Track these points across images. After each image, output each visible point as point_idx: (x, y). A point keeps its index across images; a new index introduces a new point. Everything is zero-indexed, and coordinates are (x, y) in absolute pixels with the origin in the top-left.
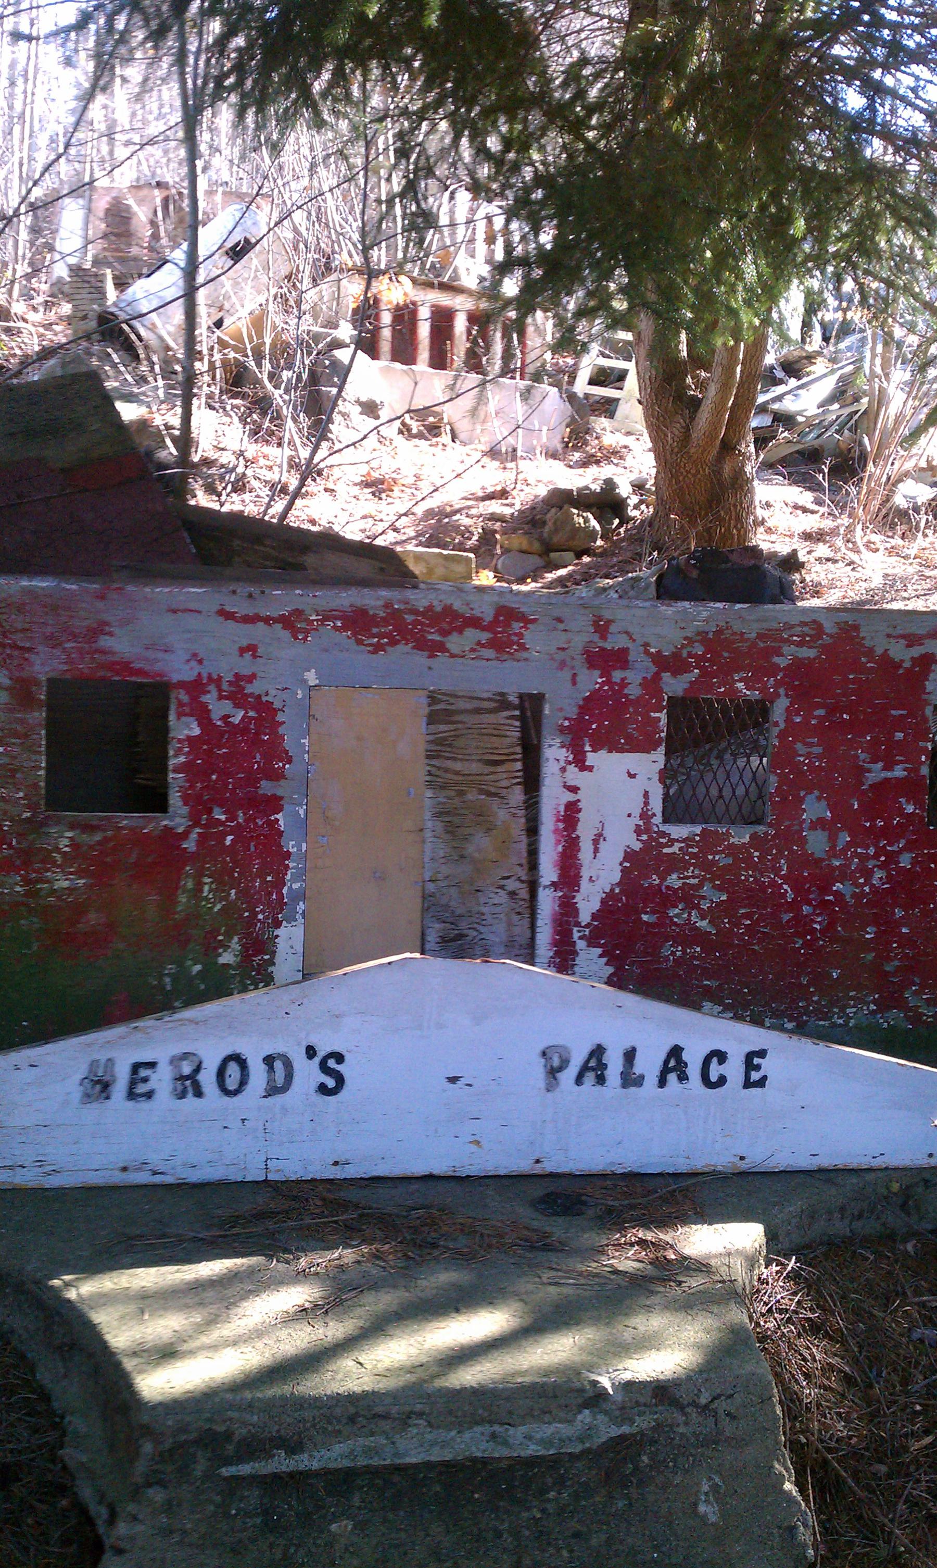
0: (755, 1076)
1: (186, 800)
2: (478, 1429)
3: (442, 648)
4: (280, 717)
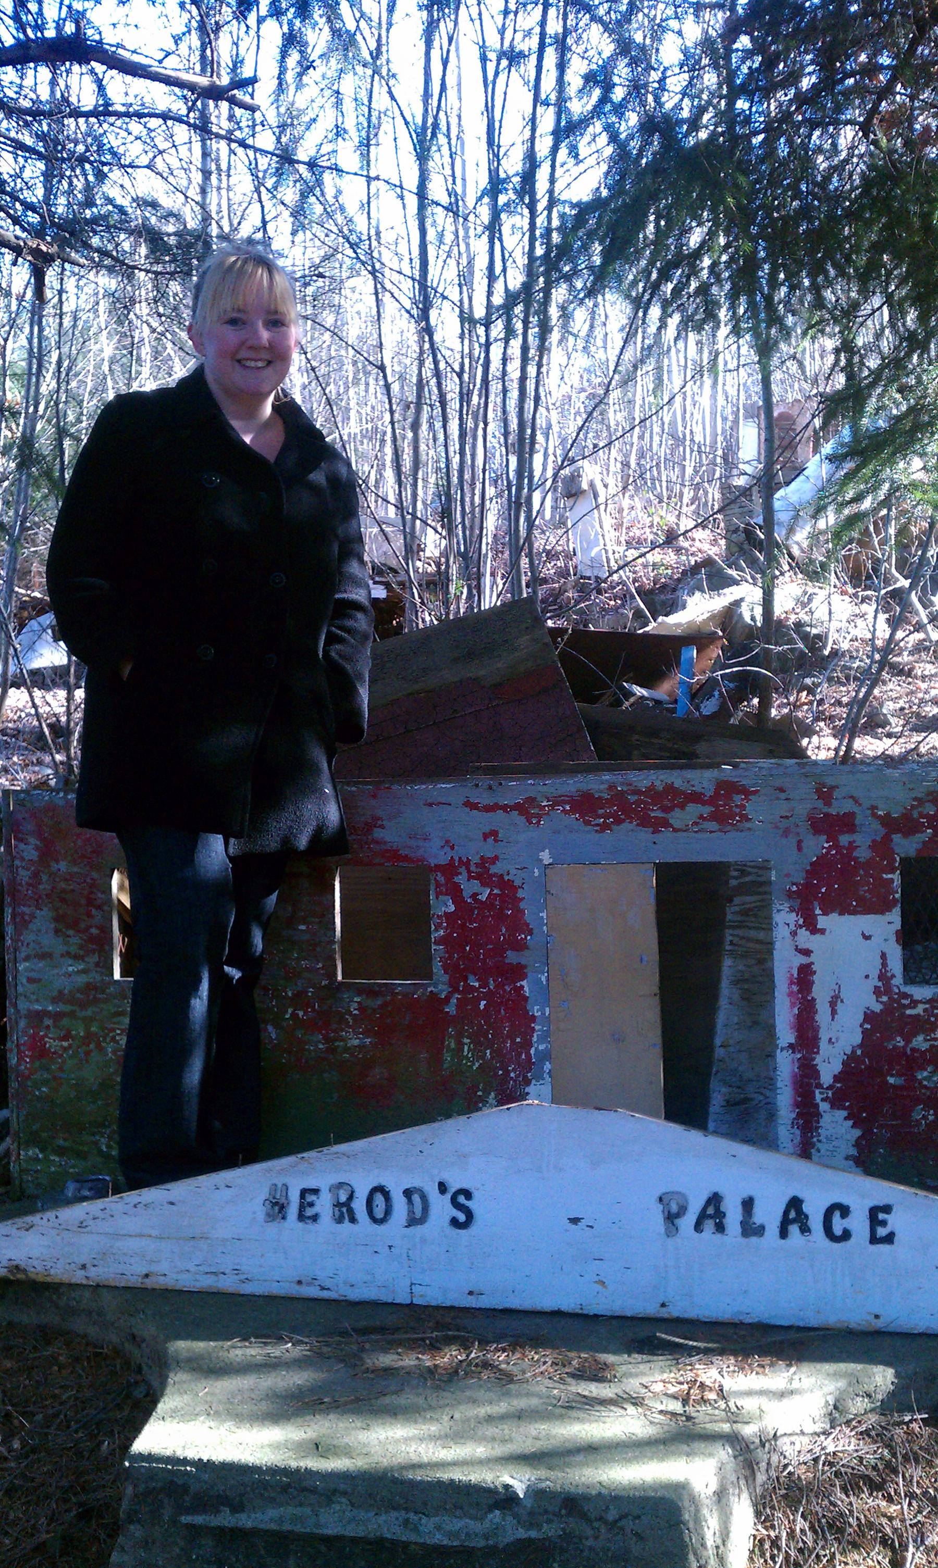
0: (882, 1232)
1: (446, 969)
2: (395, 1514)
3: (666, 824)
4: (520, 894)
